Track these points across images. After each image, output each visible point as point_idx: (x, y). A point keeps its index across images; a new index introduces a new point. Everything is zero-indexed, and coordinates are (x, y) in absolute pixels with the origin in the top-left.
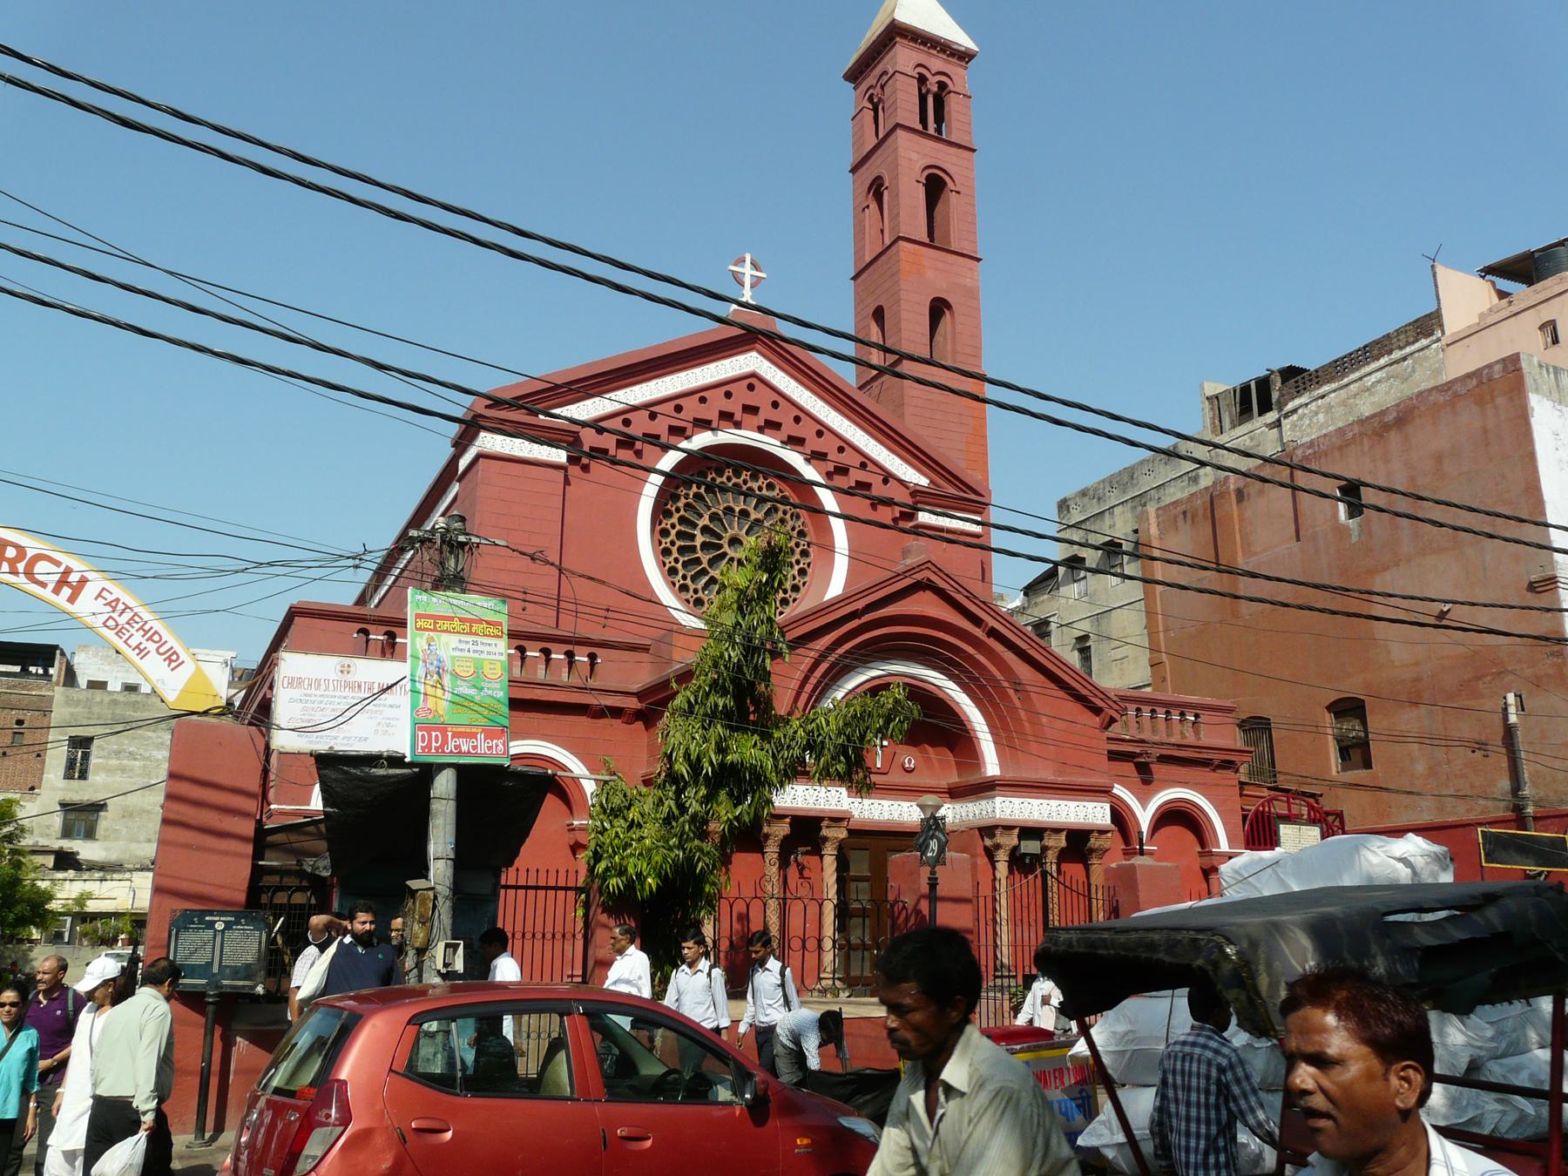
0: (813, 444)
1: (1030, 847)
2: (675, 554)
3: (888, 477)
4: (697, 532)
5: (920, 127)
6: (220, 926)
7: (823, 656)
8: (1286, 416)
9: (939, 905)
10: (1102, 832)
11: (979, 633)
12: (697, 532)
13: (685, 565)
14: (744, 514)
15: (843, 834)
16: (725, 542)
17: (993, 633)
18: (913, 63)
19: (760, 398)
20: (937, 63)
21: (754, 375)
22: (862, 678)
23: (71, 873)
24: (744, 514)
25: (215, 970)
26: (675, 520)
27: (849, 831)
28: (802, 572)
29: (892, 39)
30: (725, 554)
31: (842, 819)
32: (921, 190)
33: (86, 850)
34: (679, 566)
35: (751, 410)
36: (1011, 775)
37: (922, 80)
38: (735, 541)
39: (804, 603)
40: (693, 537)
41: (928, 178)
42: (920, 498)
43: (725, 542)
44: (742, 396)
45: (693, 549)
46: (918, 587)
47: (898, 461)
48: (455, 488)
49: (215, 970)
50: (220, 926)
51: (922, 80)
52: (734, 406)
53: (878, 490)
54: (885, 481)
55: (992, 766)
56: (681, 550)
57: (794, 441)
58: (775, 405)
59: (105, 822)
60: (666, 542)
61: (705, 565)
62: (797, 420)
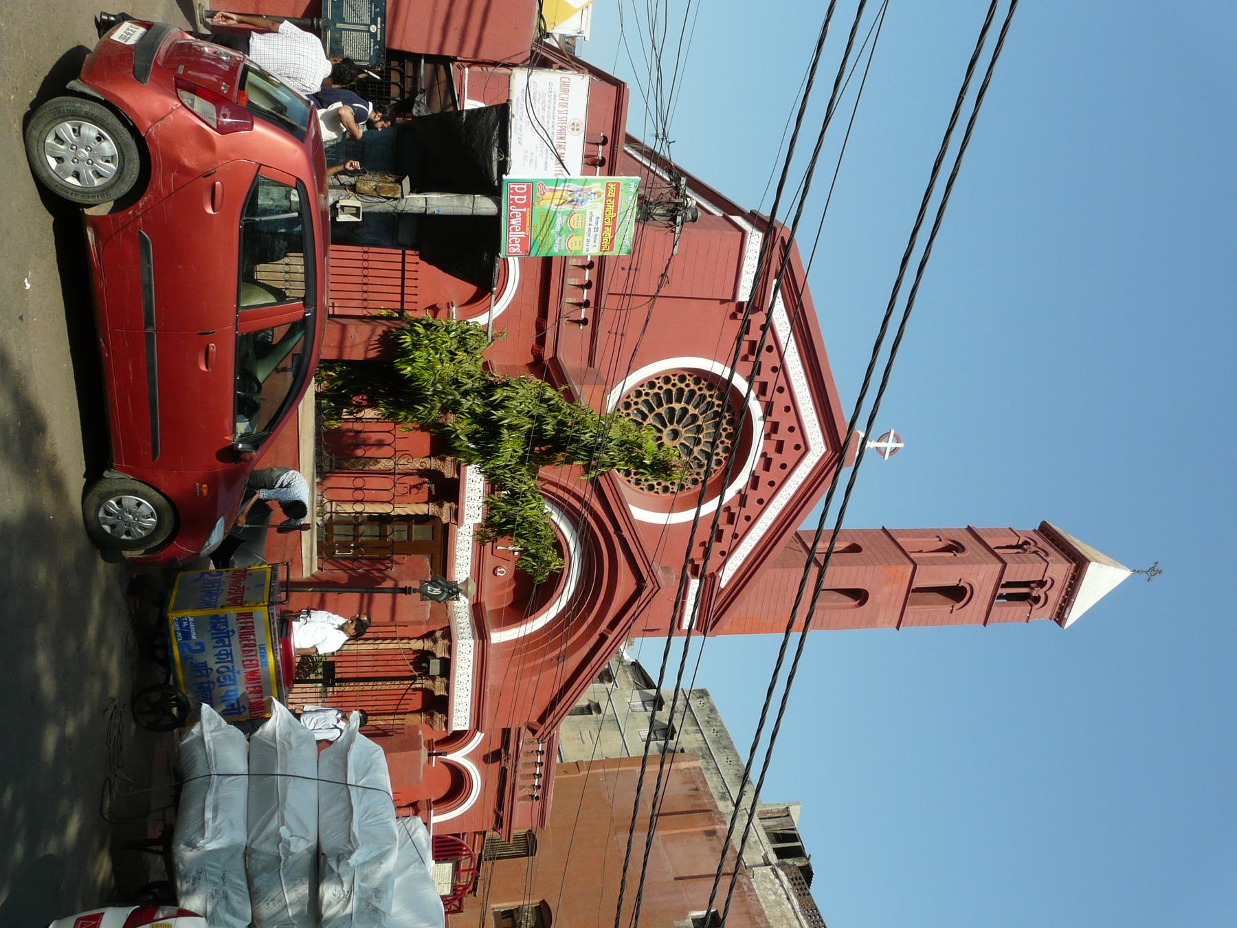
0: (753, 496)
1: (435, 667)
3: (726, 555)
5: (1003, 582)
6: (373, 29)
7: (586, 504)
8: (773, 870)
10: (446, 724)
11: (603, 627)
15: (445, 520)
17: (603, 638)
19: (789, 455)
20: (1055, 596)
21: (807, 450)
25: (339, 26)
26: (693, 387)
27: (447, 525)
35: (780, 447)
36: (491, 652)
37: (1041, 584)
38: (675, 434)
44: (791, 440)
49: (339, 26)
50: (373, 29)
51: (1041, 584)
52: (782, 434)
55: (498, 637)
56: (669, 392)
57: (754, 481)
58: (783, 466)
61: (657, 410)
62: (772, 484)
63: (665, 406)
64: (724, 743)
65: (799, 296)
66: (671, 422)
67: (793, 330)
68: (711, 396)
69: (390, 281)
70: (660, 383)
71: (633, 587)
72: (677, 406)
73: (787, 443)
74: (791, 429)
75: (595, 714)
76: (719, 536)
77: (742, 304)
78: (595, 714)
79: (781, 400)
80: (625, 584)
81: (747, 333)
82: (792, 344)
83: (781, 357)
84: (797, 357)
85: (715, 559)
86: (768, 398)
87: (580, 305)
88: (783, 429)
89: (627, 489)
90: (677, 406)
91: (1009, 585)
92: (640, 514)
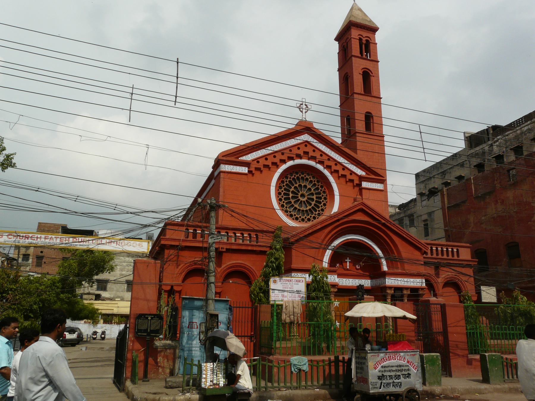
0: (327, 163)
1: (398, 294)
2: (283, 189)
3: (352, 173)
4: (290, 193)
5: (360, 56)
6: (149, 318)
7: (330, 232)
8: (494, 143)
9: (441, 330)
10: (422, 289)
11: (380, 225)
12: (291, 200)
13: (284, 194)
14: (305, 186)
15: (336, 290)
16: (300, 194)
17: (384, 225)
18: (358, 34)
19: (309, 149)
20: (365, 34)
21: (307, 142)
22: (345, 239)
23: (100, 302)
24: (305, 186)
25: (149, 331)
26: (283, 189)
27: (338, 289)
28: (325, 205)
29: (350, 27)
30: (299, 200)
31: (336, 285)
32: (361, 77)
33: (104, 294)
34: (283, 198)
35: (306, 153)
36: (391, 271)
37: (360, 40)
38: (303, 196)
39: (326, 214)
40: (289, 195)
41: (363, 72)
42: (361, 179)
43: (300, 194)
44: (303, 149)
45: (289, 191)
46: (361, 210)
47: (355, 167)
48: (213, 182)
49: (149, 331)
50: (149, 318)
51: (360, 40)
52: (301, 152)
53: (349, 177)
54: (351, 174)
55: (385, 268)
56: (285, 199)
57: (321, 163)
58: (314, 151)
59: (109, 286)
60: (280, 191)
61: (293, 203)
62: (321, 155)
63: (291, 200)
64: (438, 166)
65: (249, 147)
66: (298, 197)
67: (264, 148)
68: (286, 181)
69: (238, 312)
70: (282, 203)
71: (360, 214)
72: (291, 195)
73: (305, 150)
74: (299, 148)
75: (428, 222)
76: (344, 176)
77: (248, 171)
78: (428, 222)
79: (295, 151)
80: (360, 217)
81: (276, 163)
82: (269, 148)
83: (276, 152)
84: (274, 146)
85: (353, 177)
86: (294, 156)
87: (250, 237)
88: (267, 163)
89: (326, 214)
90: (291, 195)
91: (361, 53)
92: (335, 209)
